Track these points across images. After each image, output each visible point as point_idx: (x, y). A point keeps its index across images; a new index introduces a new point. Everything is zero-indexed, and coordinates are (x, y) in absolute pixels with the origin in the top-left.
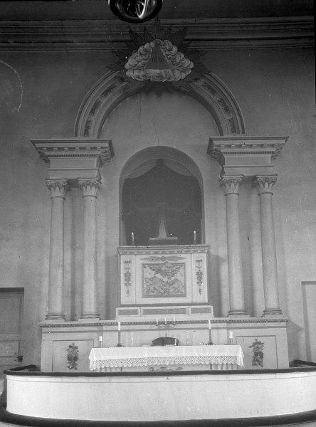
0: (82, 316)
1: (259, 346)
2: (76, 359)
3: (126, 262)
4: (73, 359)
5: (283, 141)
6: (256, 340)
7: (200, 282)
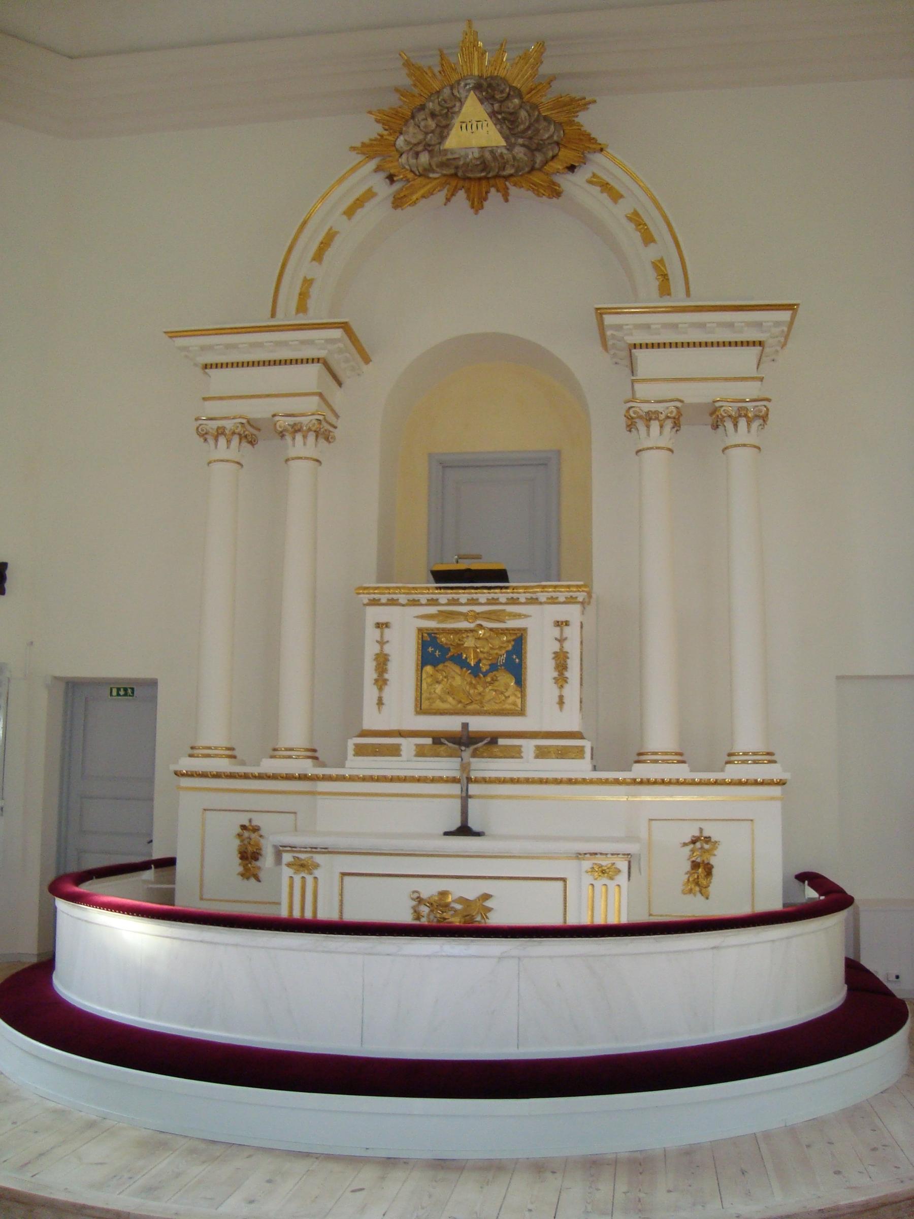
1: (706, 846)
3: (378, 625)
5: (785, 316)
6: (701, 830)
7: (561, 680)
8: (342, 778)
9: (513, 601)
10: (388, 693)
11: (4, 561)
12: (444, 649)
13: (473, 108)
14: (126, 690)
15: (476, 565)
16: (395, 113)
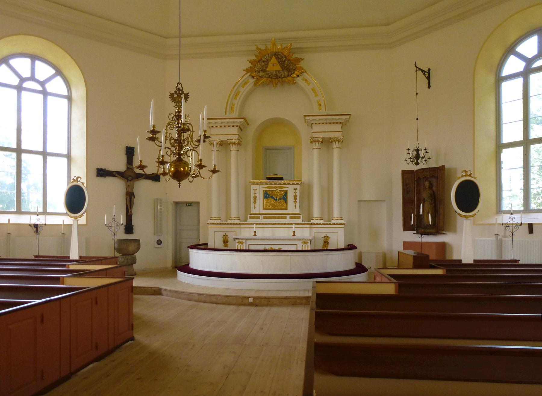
0: (230, 218)
2: (227, 242)
4: (225, 242)
5: (348, 117)
7: (295, 202)
8: (247, 224)
9: (284, 184)
10: (257, 205)
11: (99, 178)
12: (269, 195)
13: (274, 60)
14: (190, 204)
15: (276, 176)
16: (254, 60)
